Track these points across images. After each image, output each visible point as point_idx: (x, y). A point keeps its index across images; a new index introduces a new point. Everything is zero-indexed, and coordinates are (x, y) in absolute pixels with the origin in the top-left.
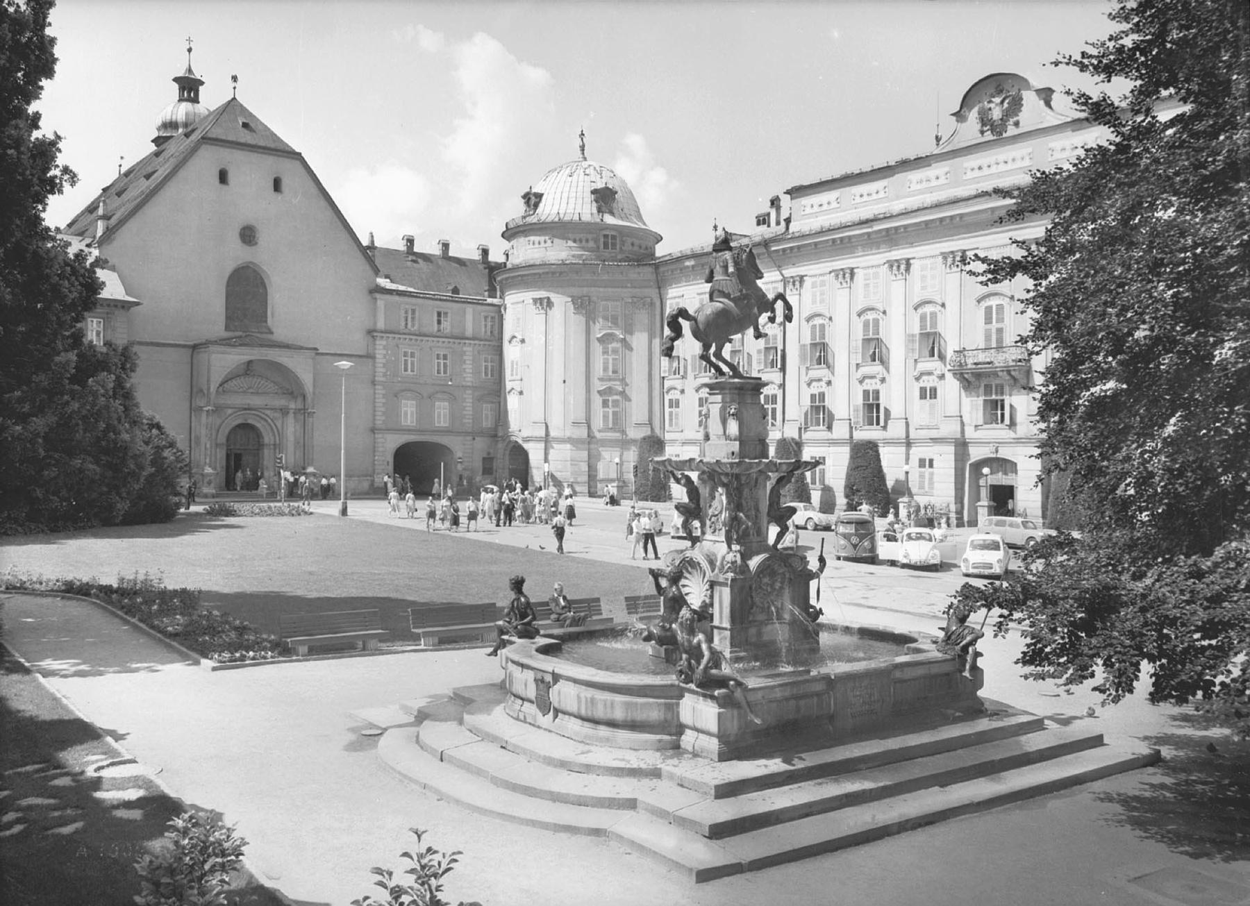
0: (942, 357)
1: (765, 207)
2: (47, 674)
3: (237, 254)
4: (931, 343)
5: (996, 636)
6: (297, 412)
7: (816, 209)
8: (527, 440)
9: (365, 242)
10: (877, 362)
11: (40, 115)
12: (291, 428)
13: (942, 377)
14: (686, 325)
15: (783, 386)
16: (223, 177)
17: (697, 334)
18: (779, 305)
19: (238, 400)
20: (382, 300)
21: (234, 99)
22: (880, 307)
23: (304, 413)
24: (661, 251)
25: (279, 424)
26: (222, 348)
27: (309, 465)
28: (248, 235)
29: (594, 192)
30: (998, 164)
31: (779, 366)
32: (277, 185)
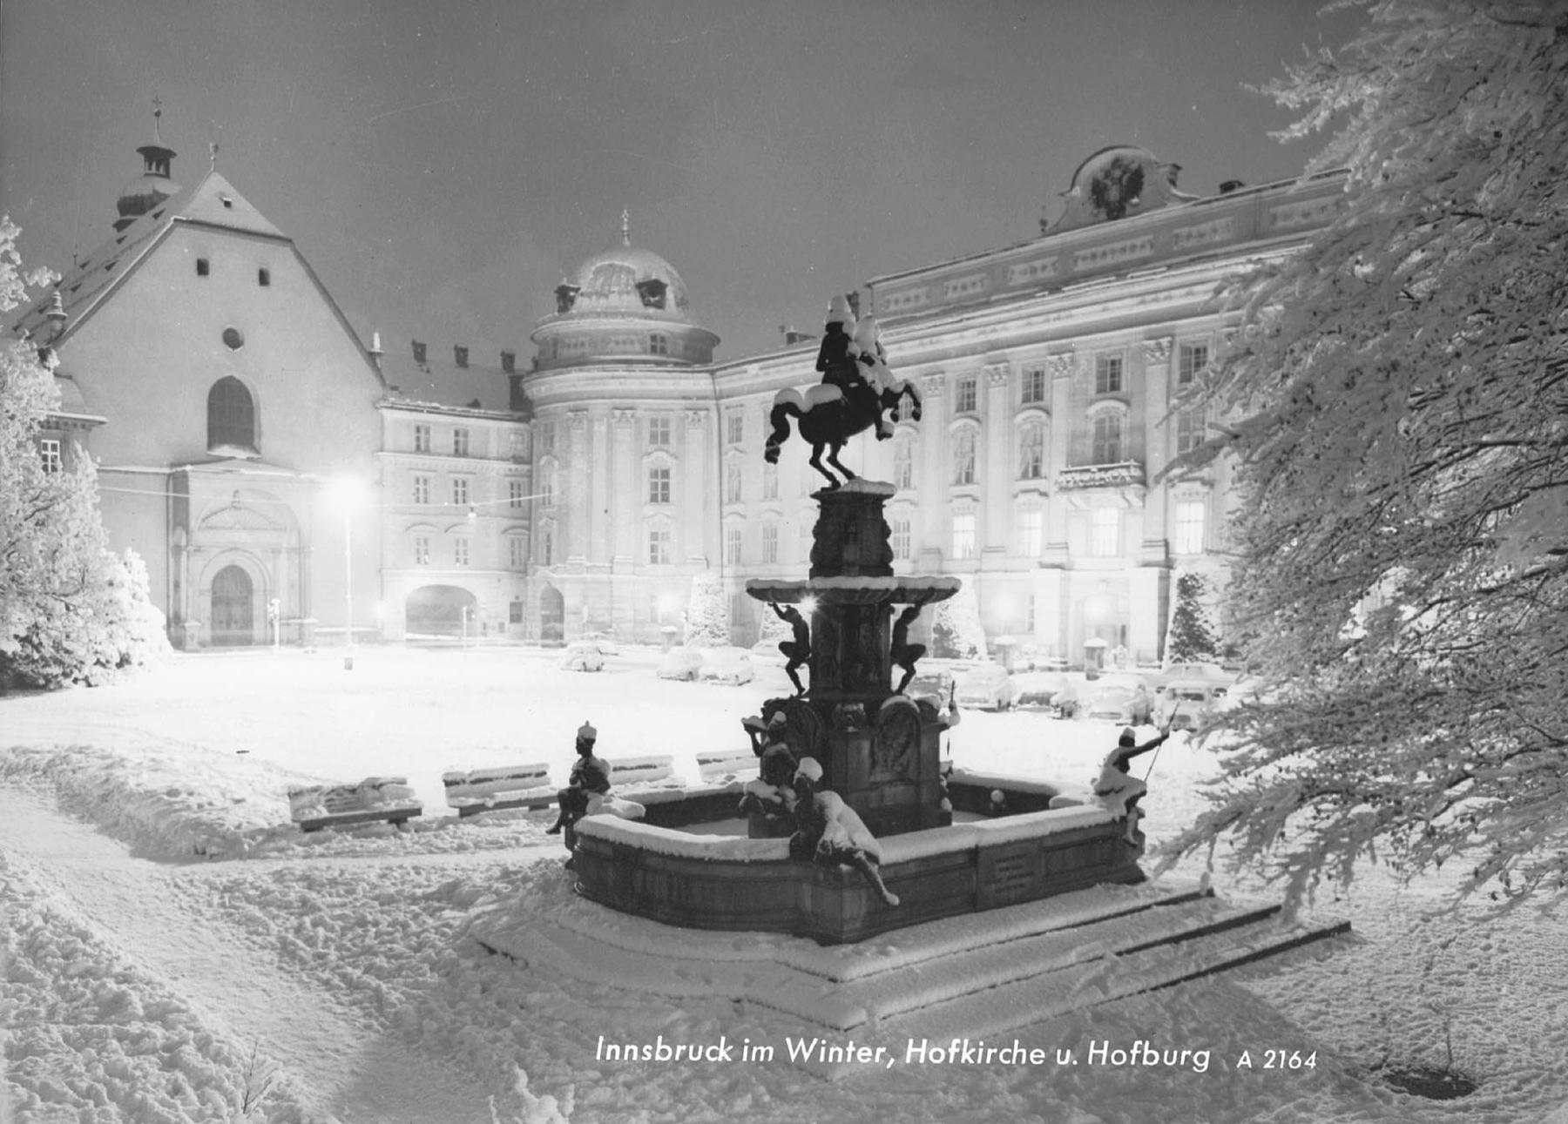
2: (544, 323)
3: (224, 364)
5: (1298, 827)
6: (290, 550)
11: (594, 731)
14: (793, 422)
16: (202, 268)
17: (806, 434)
18: (905, 401)
25: (270, 567)
32: (264, 278)
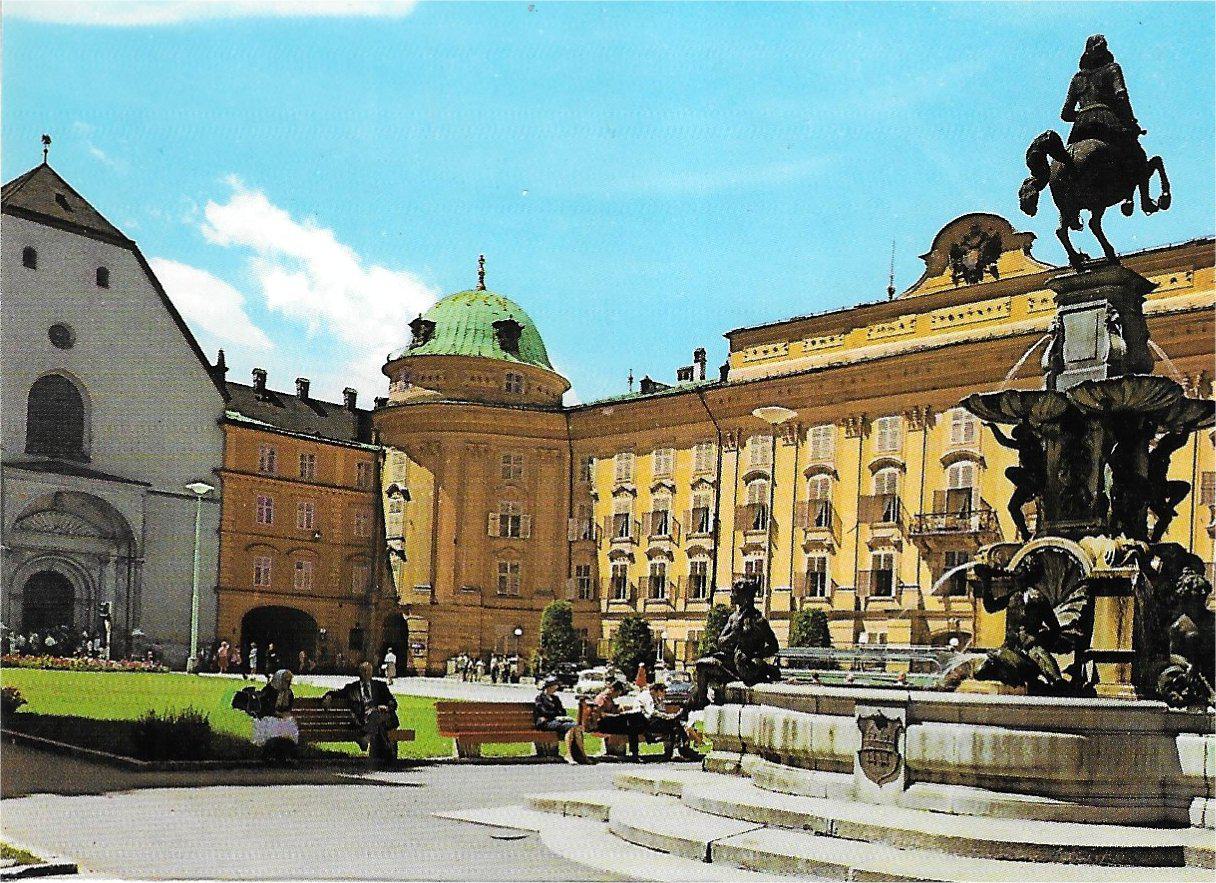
0: (899, 523)
1: (689, 361)
3: (49, 359)
4: (887, 506)
7: (761, 355)
8: (408, 608)
9: (214, 362)
10: (823, 527)
12: (111, 581)
13: (898, 546)
15: (713, 554)
19: (43, 541)
20: (233, 433)
21: (45, 165)
22: (831, 466)
23: (131, 561)
24: (570, 400)
25: (95, 575)
26: (22, 473)
27: (134, 627)
28: (61, 336)
29: (496, 325)
30: (971, 313)
31: (711, 529)
32: (102, 278)
